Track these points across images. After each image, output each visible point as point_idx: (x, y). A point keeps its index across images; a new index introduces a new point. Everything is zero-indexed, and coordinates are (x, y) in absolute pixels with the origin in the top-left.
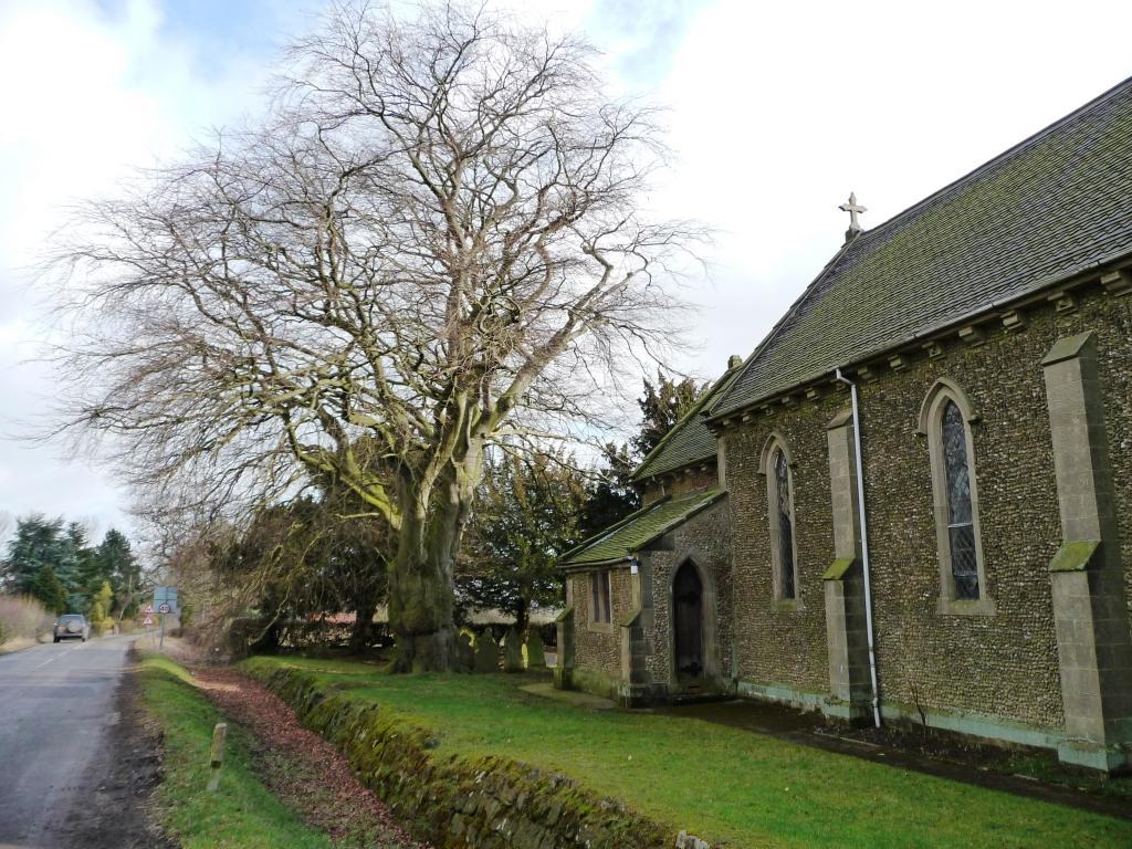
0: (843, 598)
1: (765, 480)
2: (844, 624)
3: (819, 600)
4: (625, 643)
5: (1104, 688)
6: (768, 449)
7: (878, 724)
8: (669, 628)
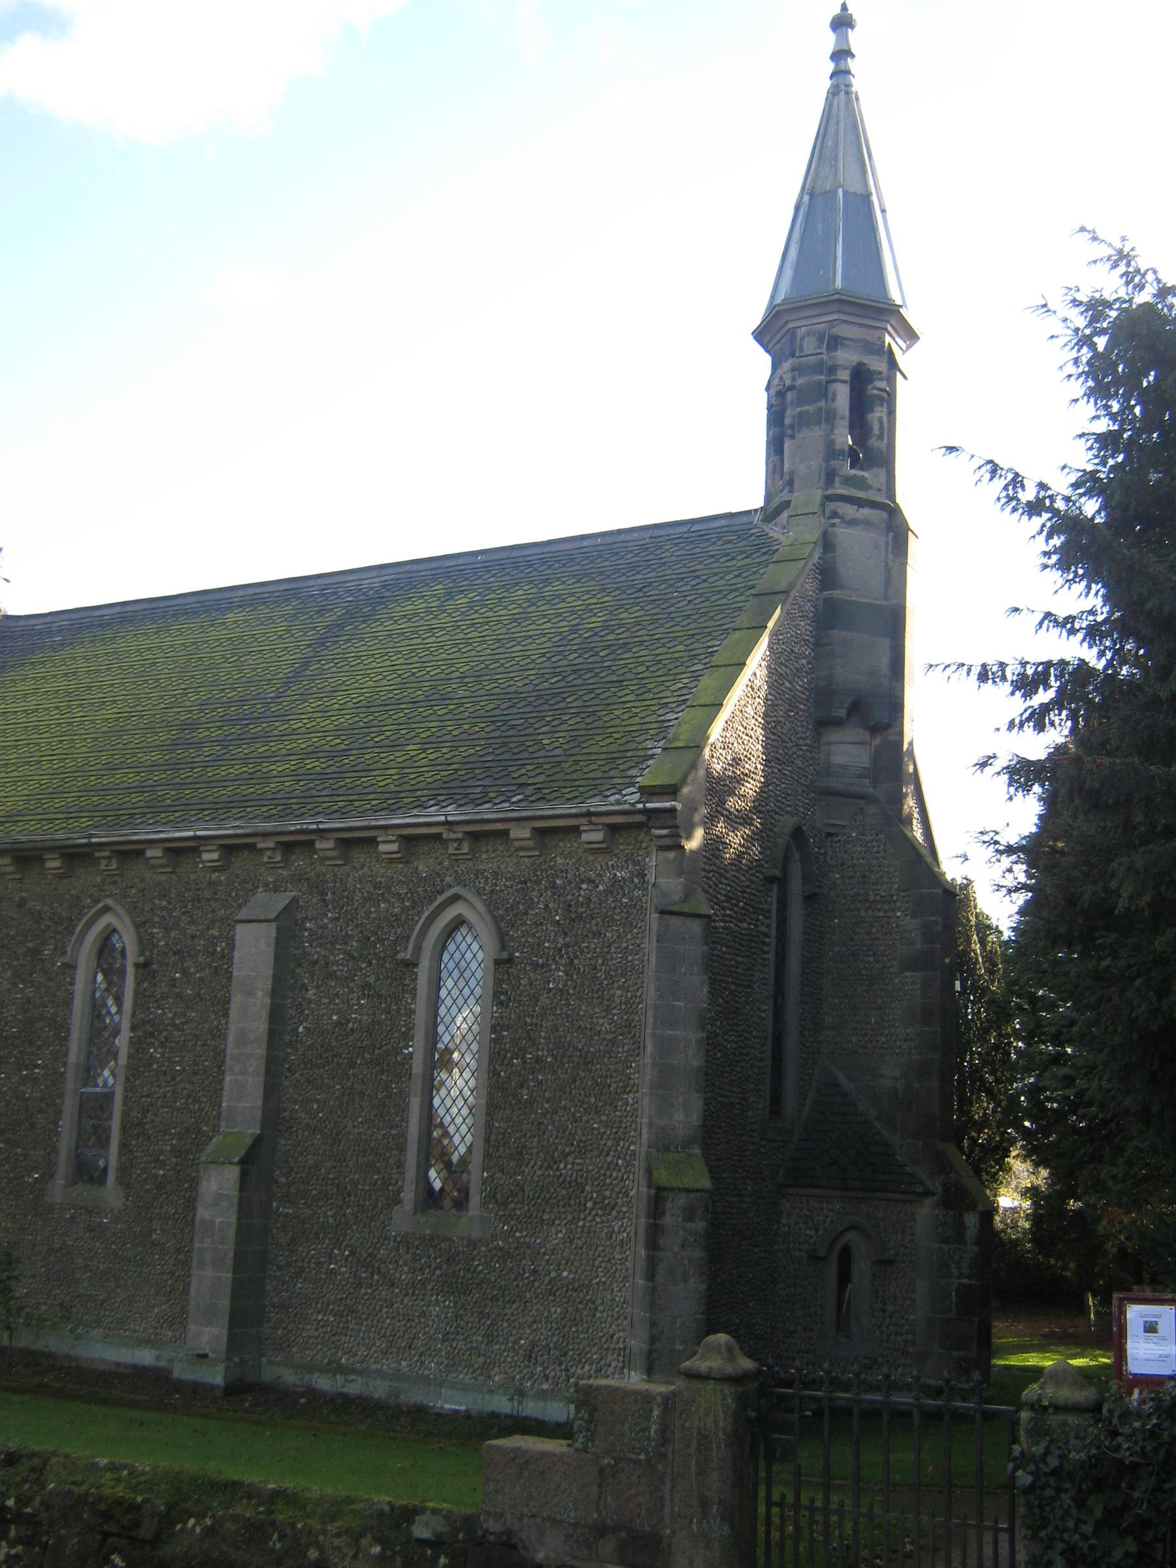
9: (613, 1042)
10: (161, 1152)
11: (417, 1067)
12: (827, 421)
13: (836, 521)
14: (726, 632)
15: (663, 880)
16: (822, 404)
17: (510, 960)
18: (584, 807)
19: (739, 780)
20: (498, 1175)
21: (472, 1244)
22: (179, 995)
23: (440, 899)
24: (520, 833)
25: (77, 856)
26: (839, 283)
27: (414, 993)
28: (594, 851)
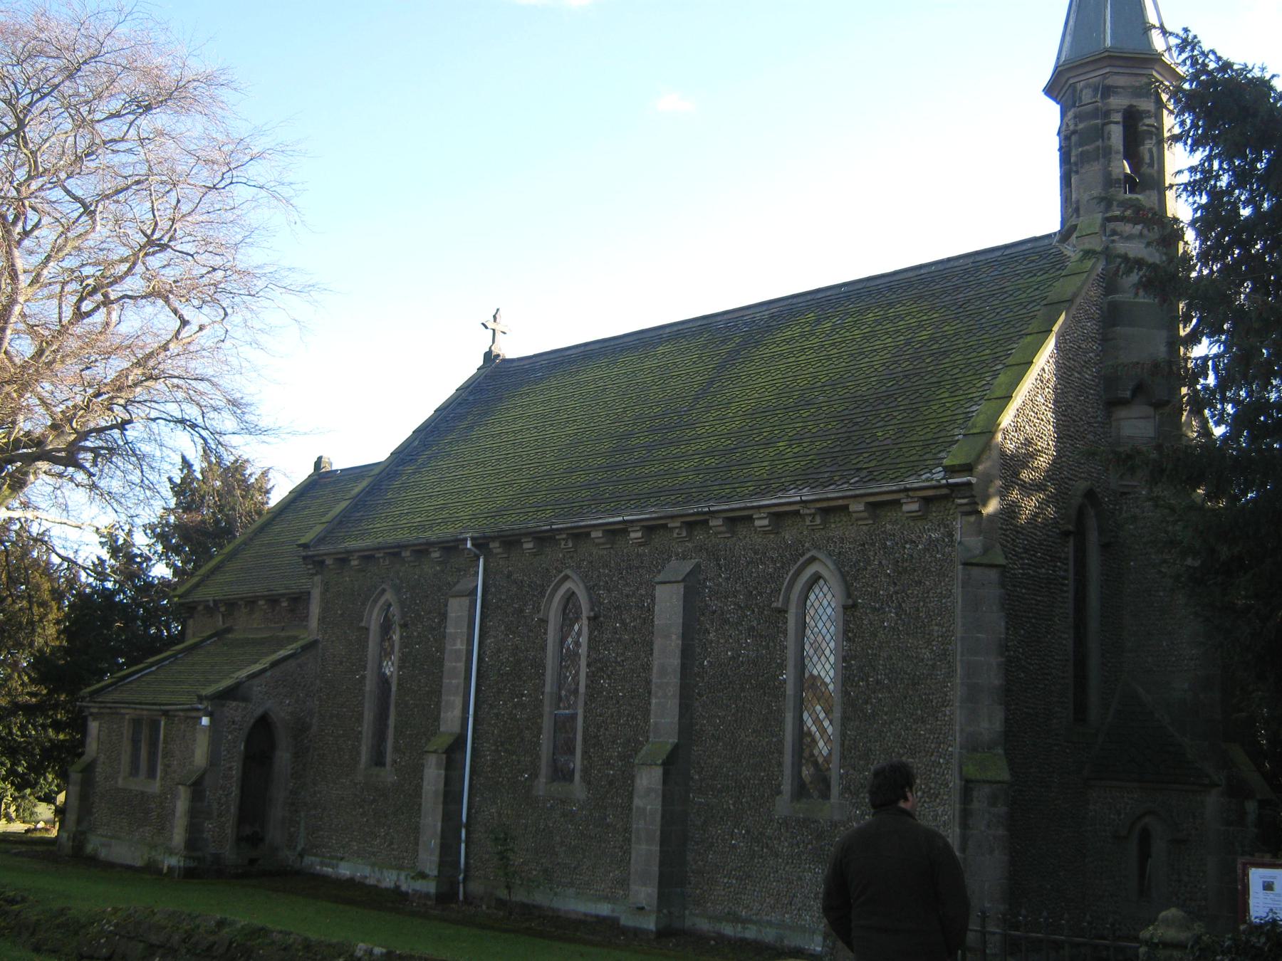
0: (443, 772)
1: (368, 634)
2: (441, 799)
3: (417, 771)
4: (181, 805)
5: (662, 864)
6: (375, 601)
7: (461, 897)
8: (235, 791)
9: (934, 666)
10: (611, 757)
11: (790, 690)
12: (1104, 157)
13: (1116, 238)
14: (1021, 337)
15: (967, 539)
16: (1099, 143)
17: (854, 606)
18: (902, 485)
19: (1033, 456)
20: (851, 771)
21: (834, 825)
22: (620, 640)
23: (802, 560)
24: (857, 507)
25: (544, 539)
26: (1108, 43)
27: (785, 633)
28: (914, 519)
